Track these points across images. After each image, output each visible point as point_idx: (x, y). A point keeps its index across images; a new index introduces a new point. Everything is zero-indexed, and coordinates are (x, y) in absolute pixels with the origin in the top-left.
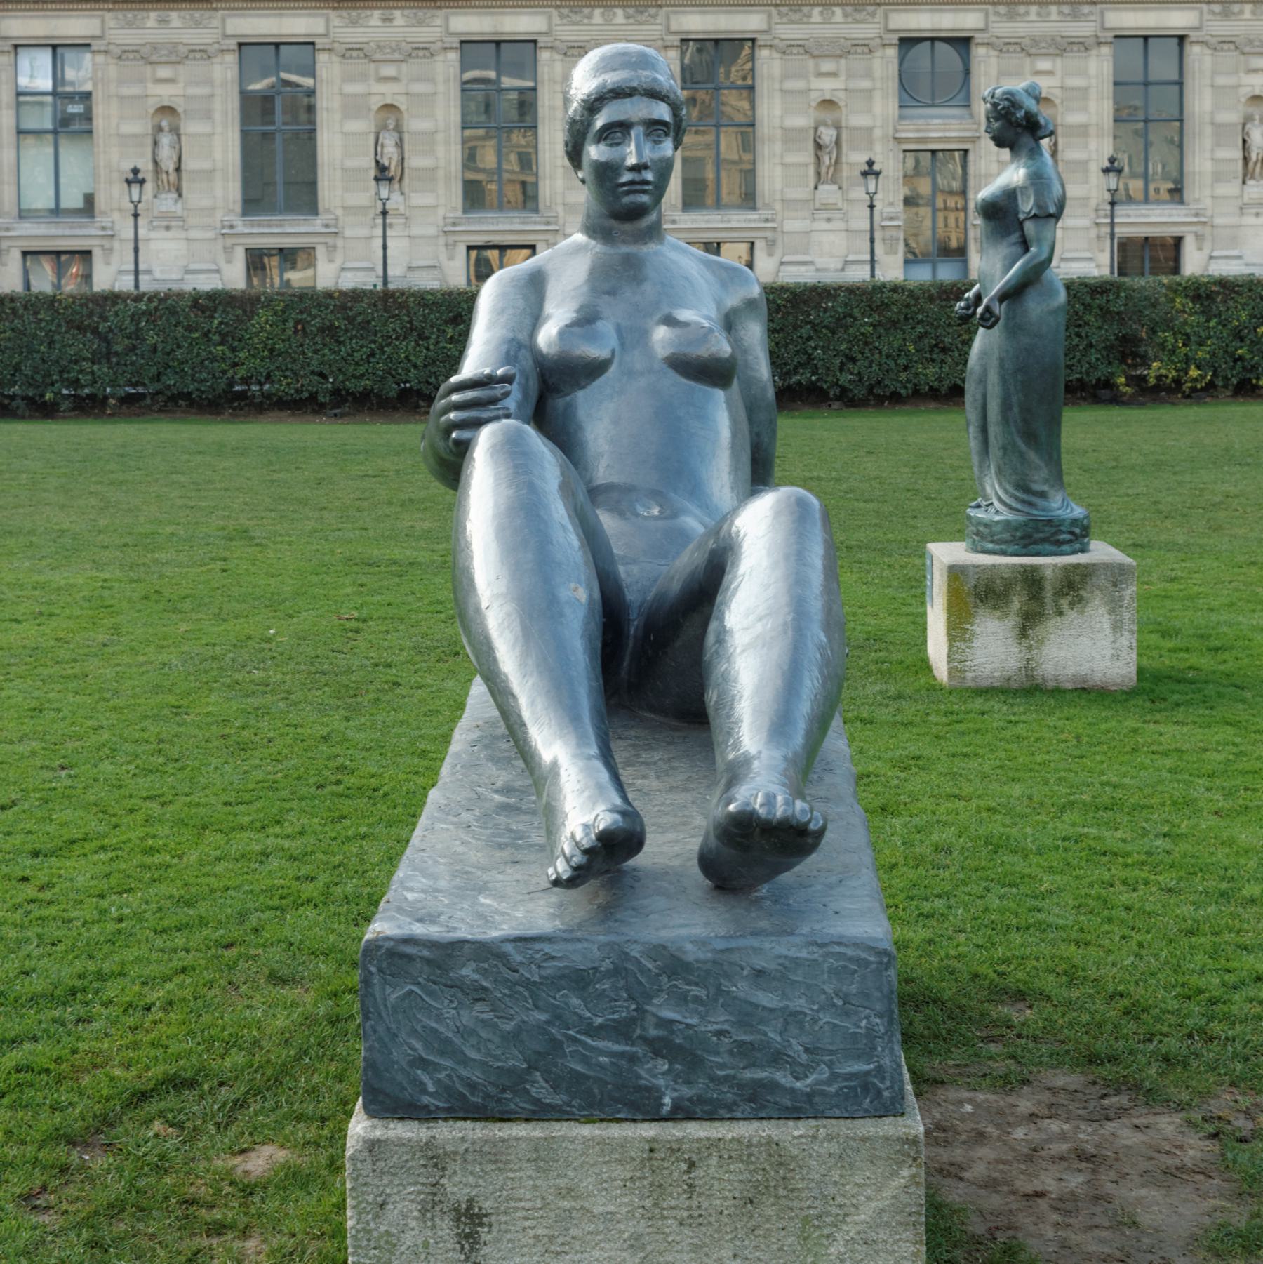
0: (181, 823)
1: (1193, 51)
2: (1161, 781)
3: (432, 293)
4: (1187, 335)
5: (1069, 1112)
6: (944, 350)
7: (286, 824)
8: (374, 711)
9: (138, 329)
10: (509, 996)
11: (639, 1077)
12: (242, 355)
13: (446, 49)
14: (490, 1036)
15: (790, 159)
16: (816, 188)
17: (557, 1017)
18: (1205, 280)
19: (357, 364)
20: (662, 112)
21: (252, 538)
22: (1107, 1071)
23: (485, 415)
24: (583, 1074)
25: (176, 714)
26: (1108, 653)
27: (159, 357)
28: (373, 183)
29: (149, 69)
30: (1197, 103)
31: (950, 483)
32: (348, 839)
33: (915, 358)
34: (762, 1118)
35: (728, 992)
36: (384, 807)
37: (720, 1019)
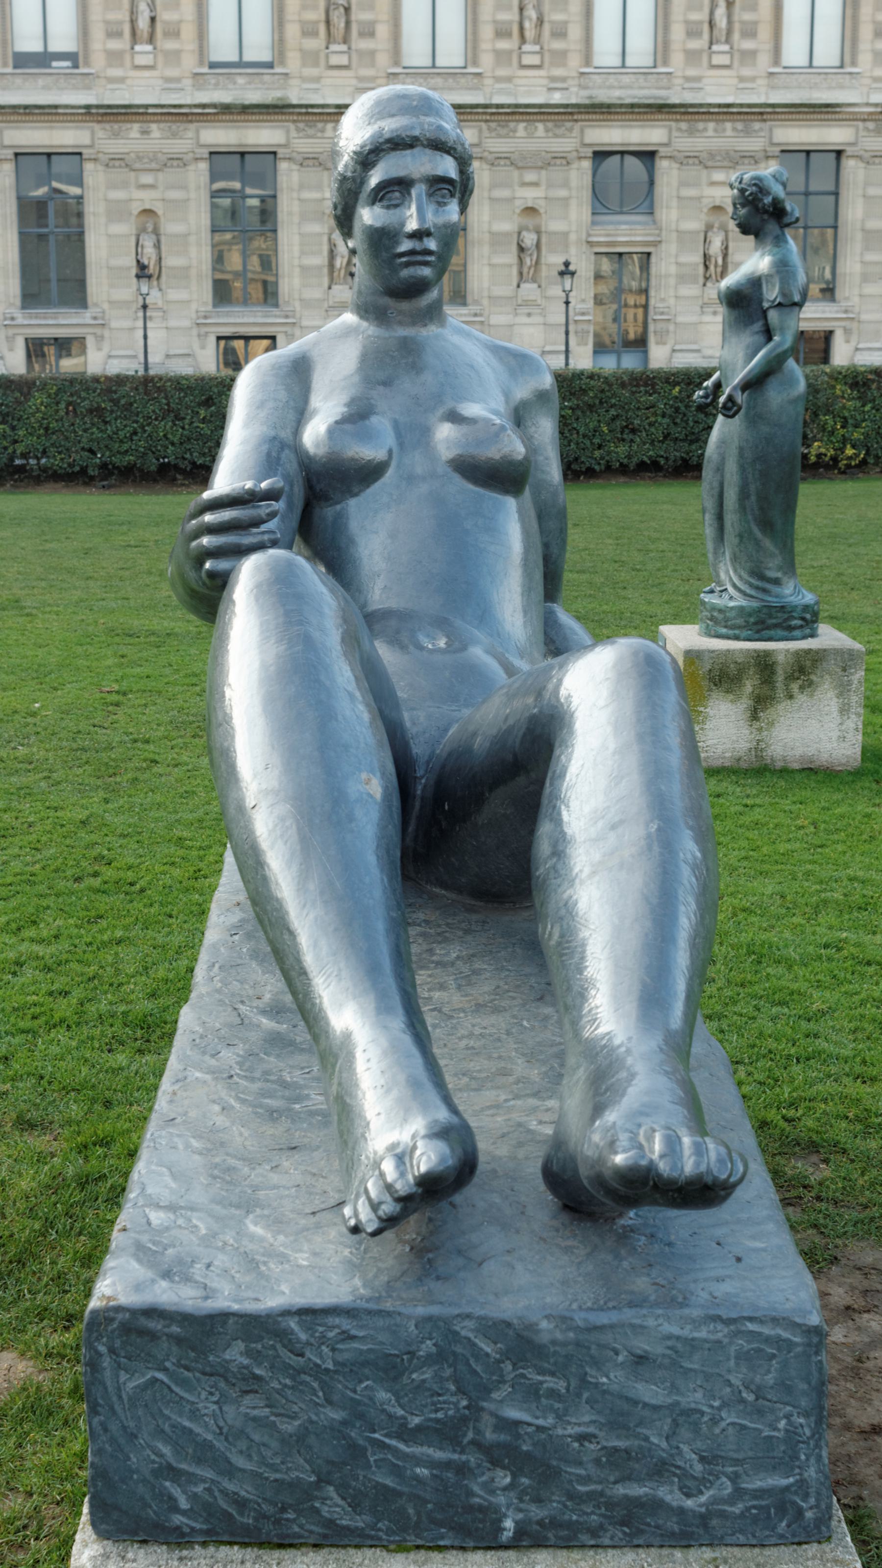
1: (849, 165)
3: (186, 378)
4: (845, 418)
6: (633, 431)
7: (42, 925)
8: (133, 792)
11: (470, 1494)
12: (21, 433)
13: (197, 159)
14: (266, 1439)
16: (518, 286)
18: (863, 369)
19: (121, 441)
20: (448, 167)
23: (246, 540)
24: (394, 1490)
26: (835, 734)
28: (135, 280)
30: (850, 210)
31: (652, 555)
32: (104, 944)
33: (608, 438)
34: (638, 1546)
35: (597, 1385)
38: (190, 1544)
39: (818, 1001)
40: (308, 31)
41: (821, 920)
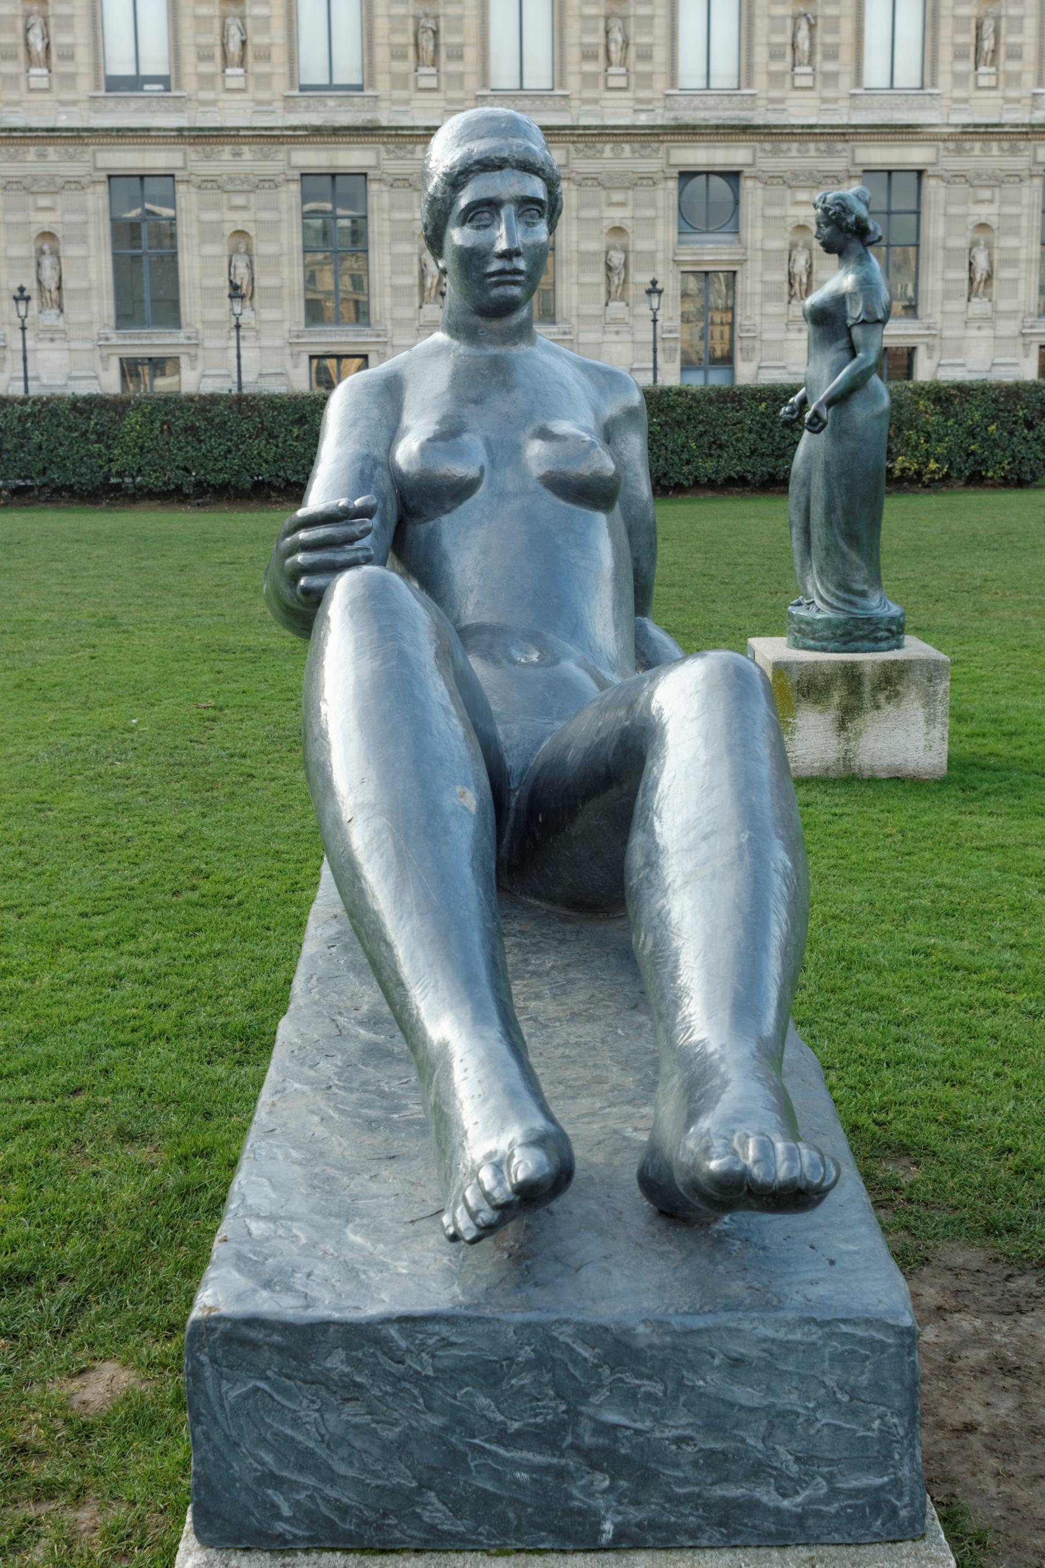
0: (35, 939)
1: (930, 184)
2: (993, 883)
3: (279, 397)
4: (928, 433)
5: (976, 1301)
6: (721, 447)
7: (141, 939)
9: (25, 430)
10: (393, 1395)
11: (570, 1497)
12: (116, 452)
13: (288, 181)
14: (367, 1446)
15: (586, 279)
17: (458, 1419)
19: (216, 460)
20: (536, 188)
21: (119, 625)
22: (1006, 1244)
23: (341, 557)
24: (494, 1495)
25: (40, 811)
26: (922, 744)
27: (44, 454)
28: (228, 300)
29: (30, 198)
31: (740, 568)
32: (203, 957)
34: (735, 1546)
35: (693, 1388)
36: (238, 919)
39: (908, 1006)
40: (398, 55)
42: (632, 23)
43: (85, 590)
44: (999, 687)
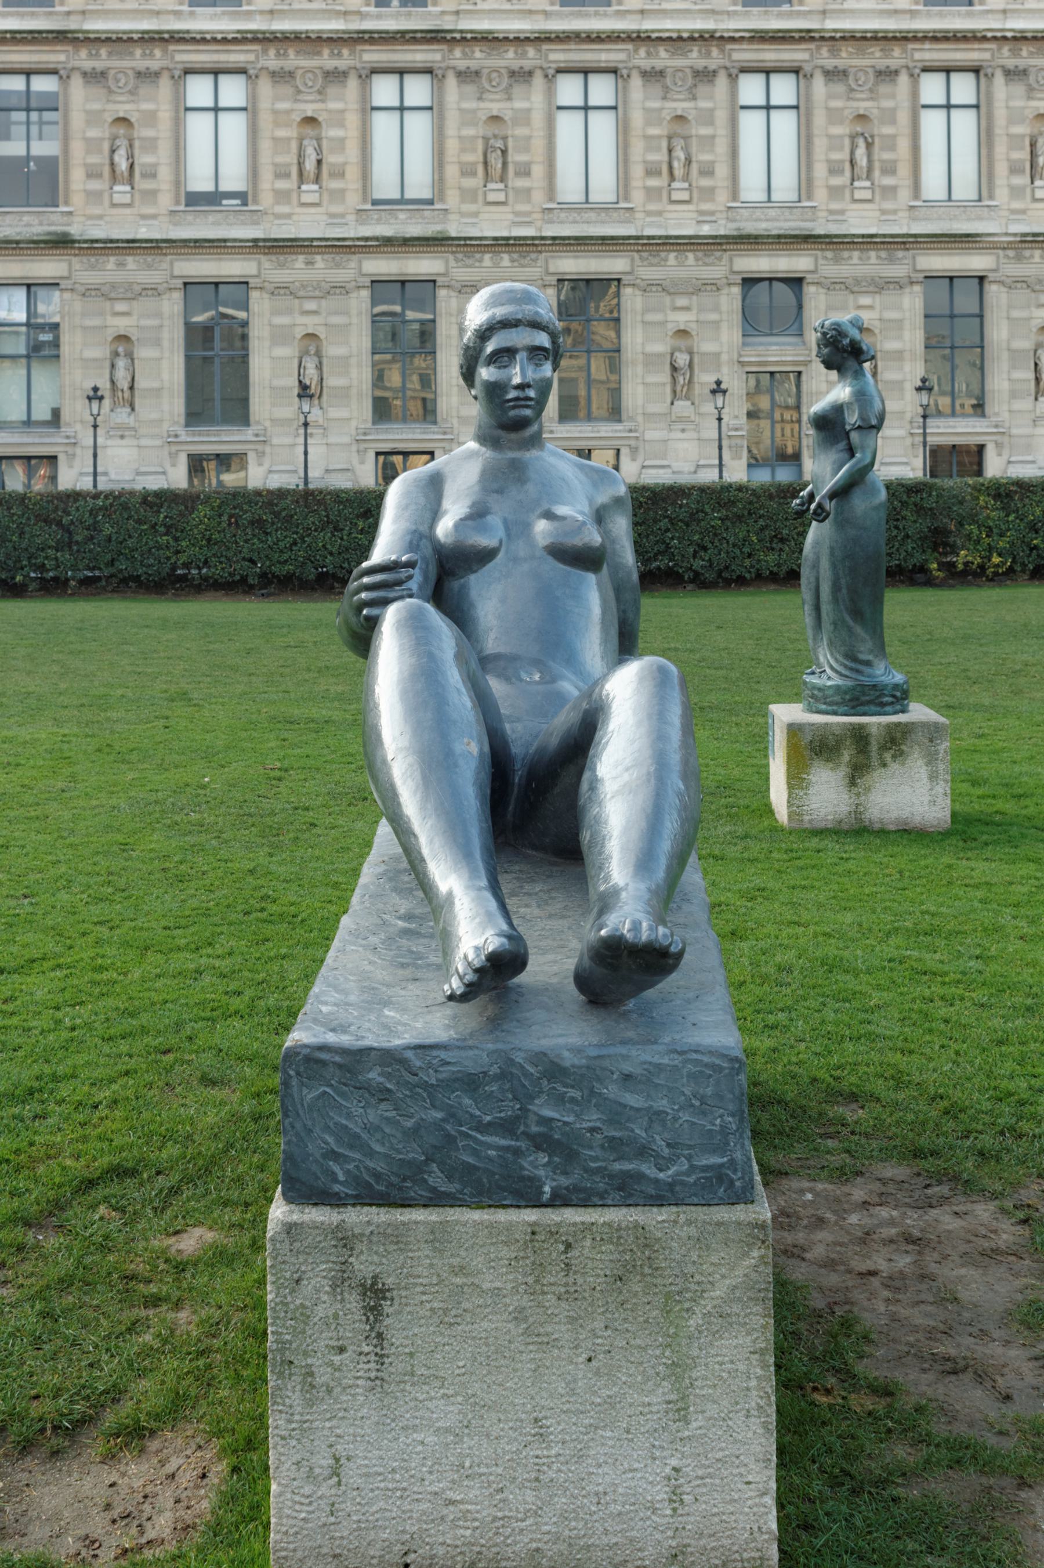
0: (126, 944)
3: (346, 491)
4: (990, 527)
6: (782, 540)
9: (96, 522)
11: (522, 1168)
12: (184, 544)
14: (394, 1132)
17: (451, 1115)
19: (281, 551)
20: (543, 339)
21: (190, 700)
23: (391, 595)
24: (474, 1166)
26: (926, 799)
27: (113, 545)
28: (297, 399)
29: (108, 304)
32: (271, 959)
36: (302, 932)
37: (593, 1118)
38: (345, 1205)
39: (876, 998)
40: (467, 171)
41: (890, 942)
42: (694, 142)
43: (157, 670)
44: (1017, 757)
